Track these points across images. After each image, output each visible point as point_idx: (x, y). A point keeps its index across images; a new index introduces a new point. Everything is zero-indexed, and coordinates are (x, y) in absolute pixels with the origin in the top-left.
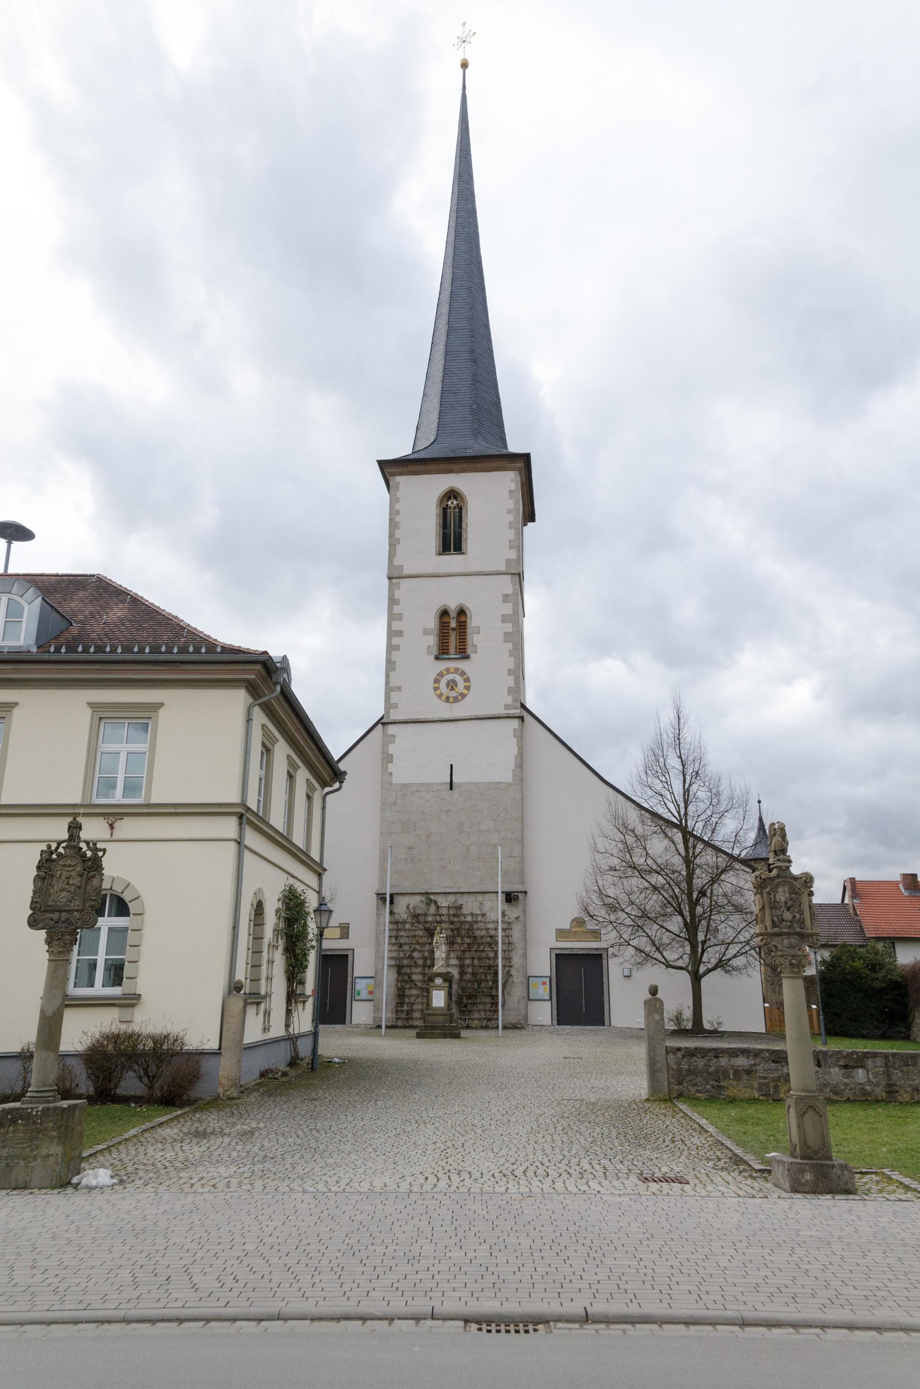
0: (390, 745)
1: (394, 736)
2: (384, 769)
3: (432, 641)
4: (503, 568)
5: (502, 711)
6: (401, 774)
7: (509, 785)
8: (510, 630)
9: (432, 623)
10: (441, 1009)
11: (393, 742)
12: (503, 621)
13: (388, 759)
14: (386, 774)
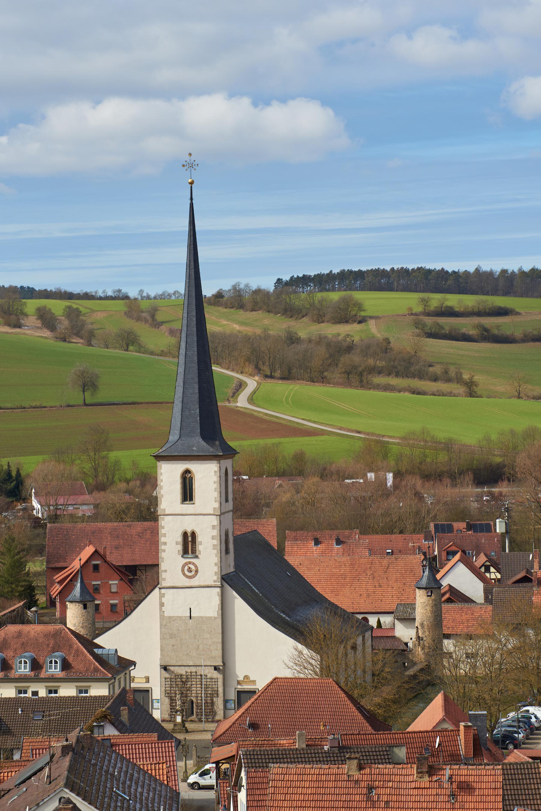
0: (163, 598)
1: (164, 594)
2: (161, 609)
3: (180, 547)
4: (212, 512)
5: (213, 584)
6: (169, 612)
7: (215, 618)
8: (216, 543)
9: (180, 539)
10: (179, 723)
11: (164, 597)
12: (213, 539)
13: (162, 605)
14: (162, 612)
